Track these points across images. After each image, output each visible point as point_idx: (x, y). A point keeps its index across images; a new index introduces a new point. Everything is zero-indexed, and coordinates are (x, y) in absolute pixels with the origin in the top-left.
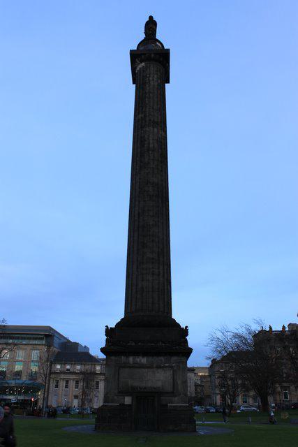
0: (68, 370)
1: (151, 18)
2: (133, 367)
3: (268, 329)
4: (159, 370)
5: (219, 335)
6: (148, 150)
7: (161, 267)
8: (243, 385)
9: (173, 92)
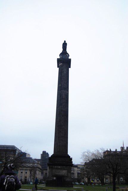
0: (36, 166)
1: (65, 41)
2: (56, 169)
3: (109, 150)
4: (64, 170)
5: (86, 154)
7: (65, 139)
8: (93, 174)
9: (72, 71)
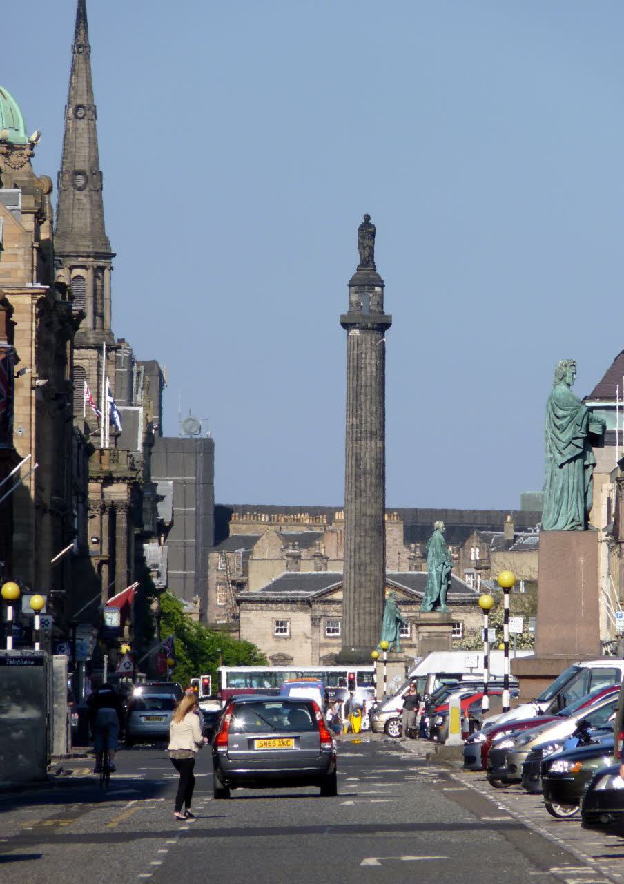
6: (365, 474)
